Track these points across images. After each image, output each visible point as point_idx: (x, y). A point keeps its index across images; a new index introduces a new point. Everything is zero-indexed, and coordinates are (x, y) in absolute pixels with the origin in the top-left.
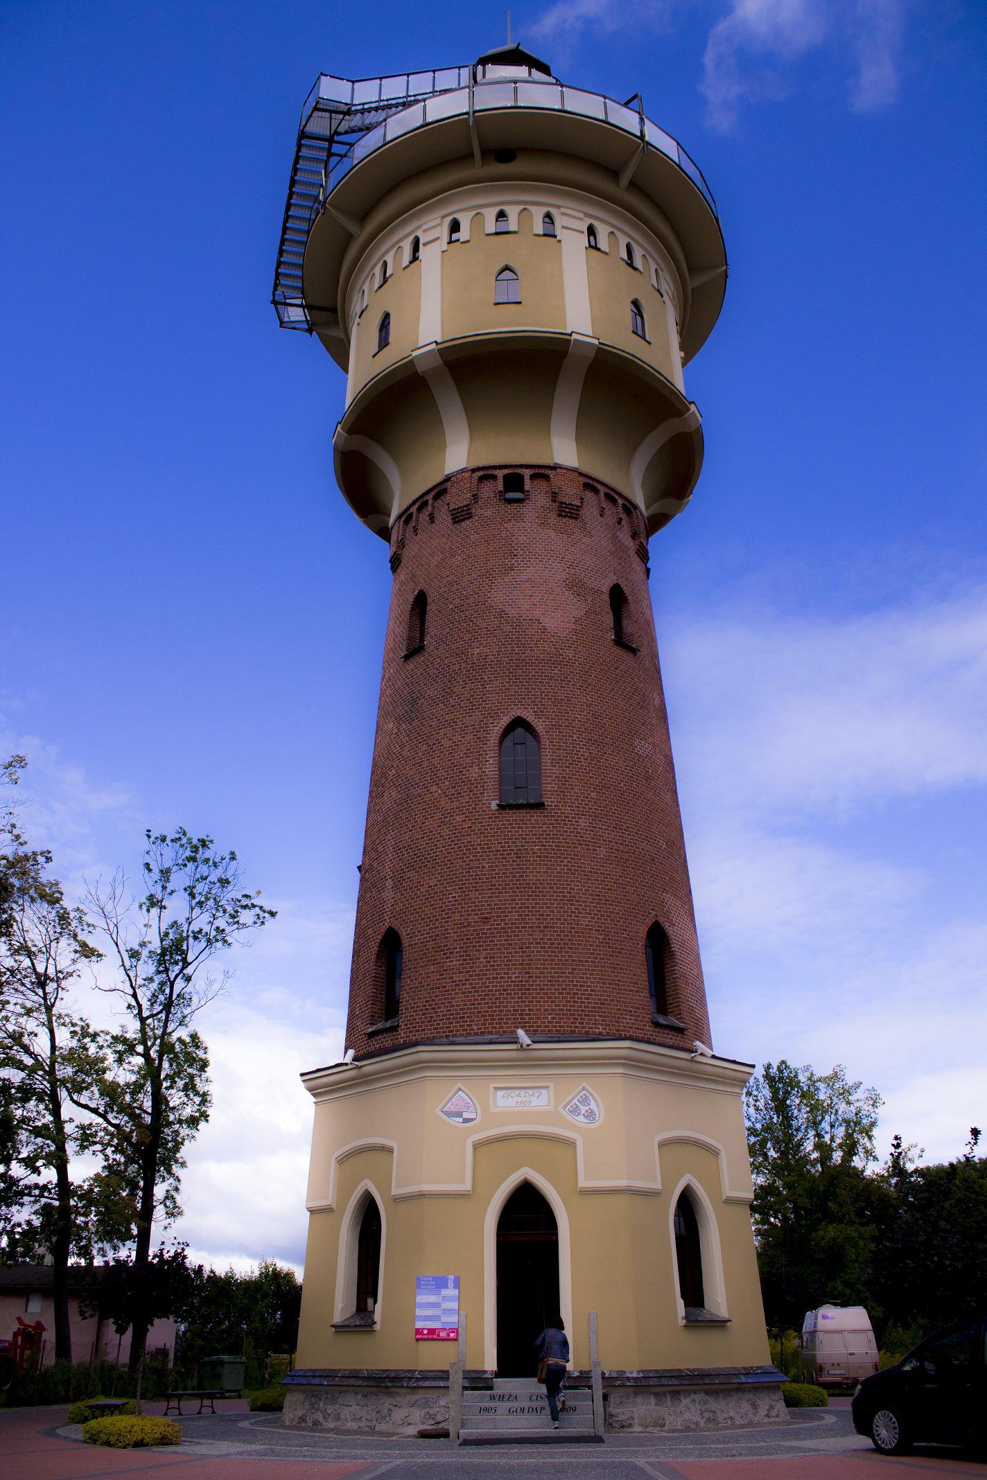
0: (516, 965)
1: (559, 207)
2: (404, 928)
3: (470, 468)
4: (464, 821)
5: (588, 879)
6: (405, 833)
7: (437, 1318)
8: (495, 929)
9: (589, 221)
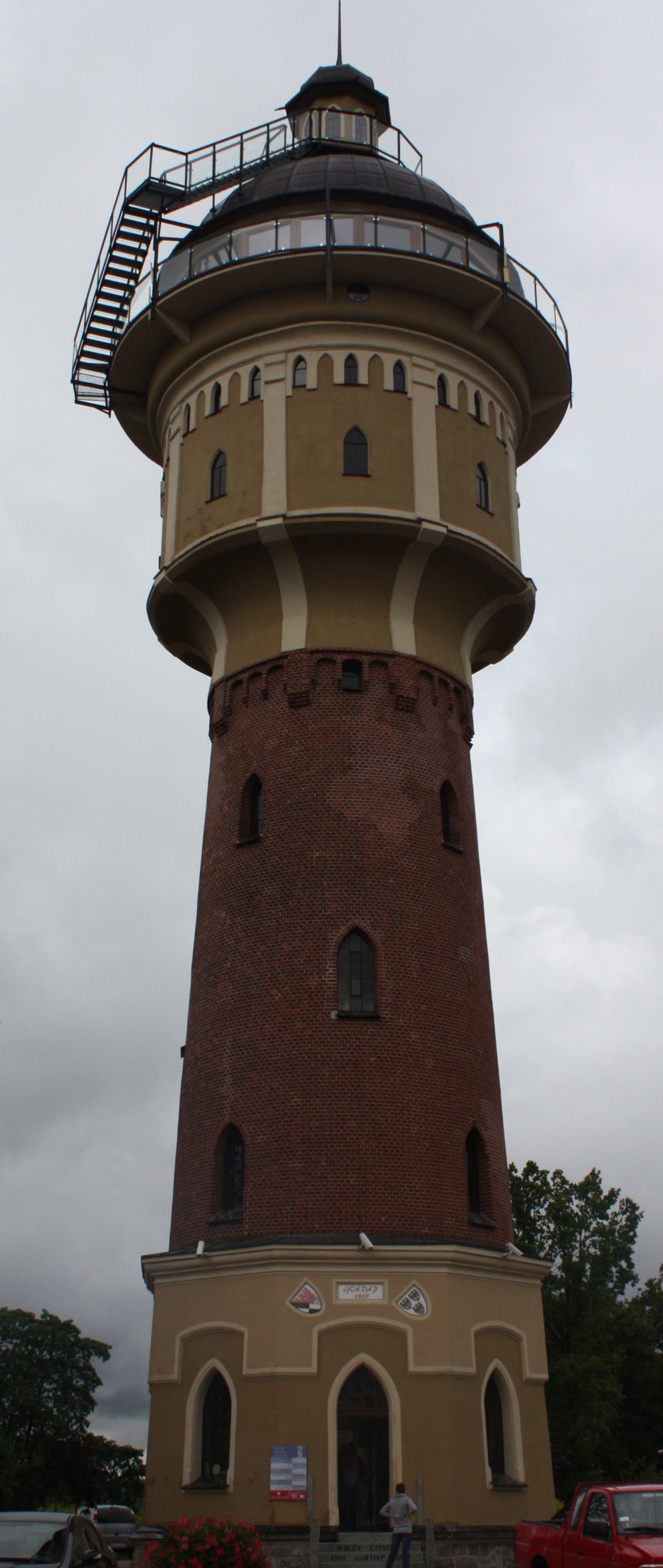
0: (353, 1169)
1: (410, 355)
2: (246, 1126)
3: (309, 650)
4: (305, 1028)
5: (418, 1090)
6: (245, 1031)
7: (288, 1482)
8: (335, 1135)
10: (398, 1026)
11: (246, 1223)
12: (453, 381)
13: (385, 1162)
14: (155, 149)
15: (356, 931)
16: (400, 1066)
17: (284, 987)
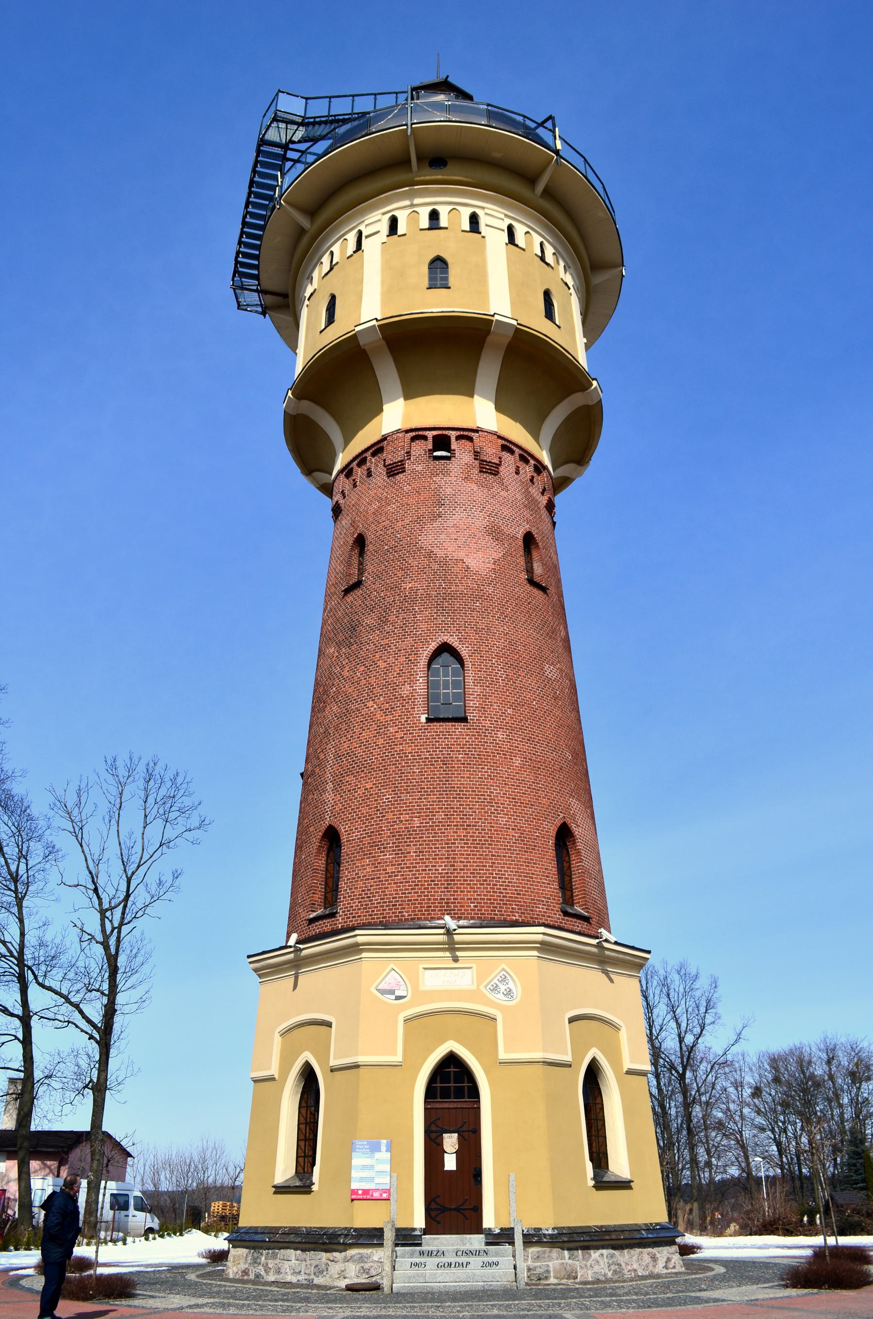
0: (442, 859)
1: (483, 208)
2: (343, 825)
7: (371, 1179)
9: (508, 221)
10: (485, 726)
11: (340, 916)
12: (520, 230)
13: (474, 851)
14: (280, 94)
15: (445, 648)
16: (488, 762)
17: (379, 699)
